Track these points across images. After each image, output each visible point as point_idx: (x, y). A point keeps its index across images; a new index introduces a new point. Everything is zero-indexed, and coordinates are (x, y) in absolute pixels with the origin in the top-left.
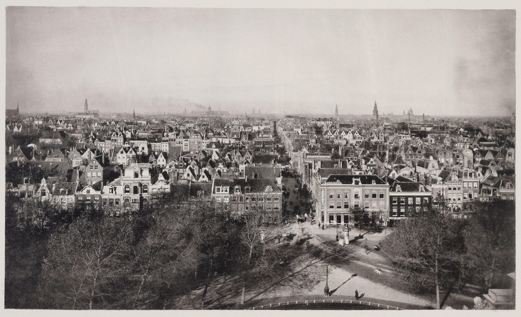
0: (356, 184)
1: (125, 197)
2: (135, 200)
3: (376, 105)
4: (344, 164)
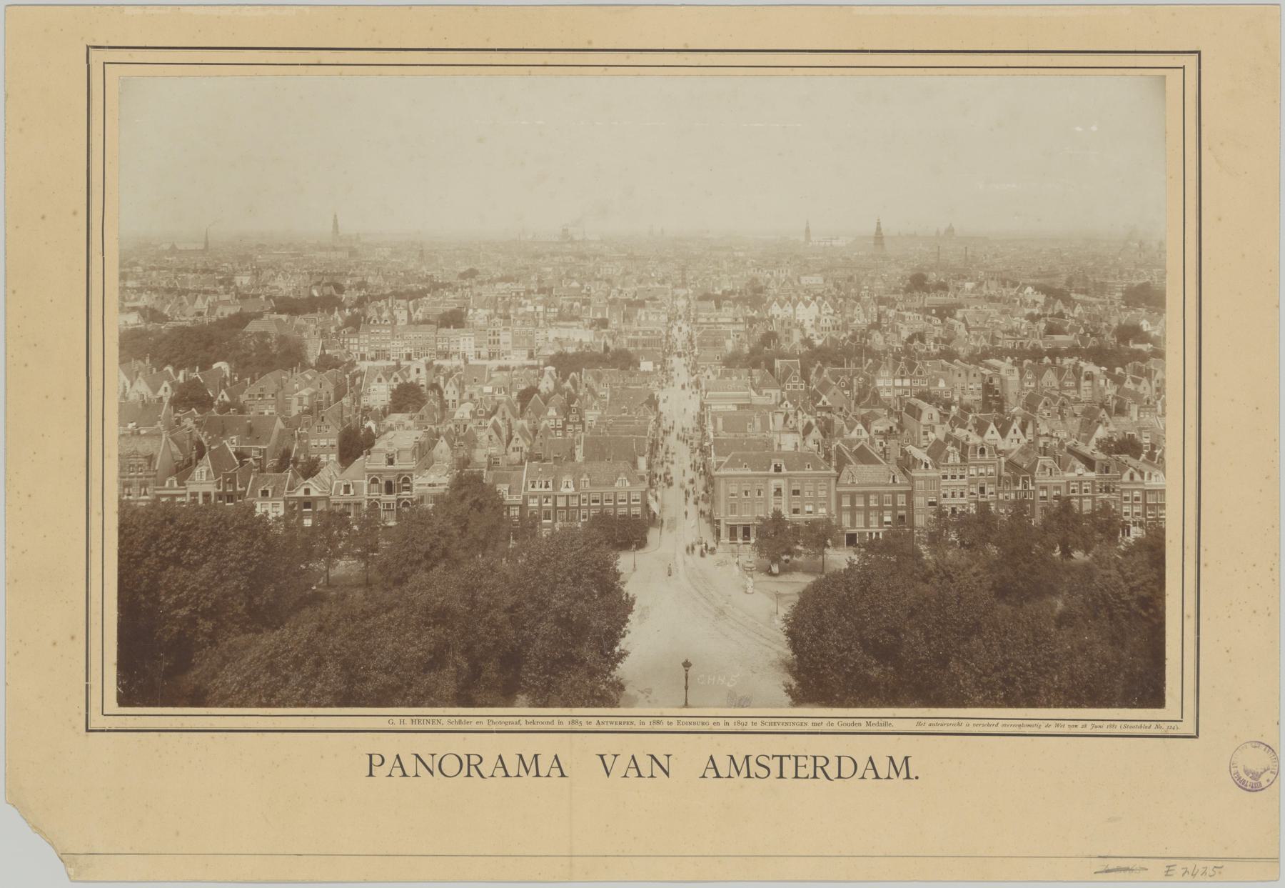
0: (776, 471)
1: (372, 500)
2: (388, 505)
3: (879, 223)
4: (765, 426)
